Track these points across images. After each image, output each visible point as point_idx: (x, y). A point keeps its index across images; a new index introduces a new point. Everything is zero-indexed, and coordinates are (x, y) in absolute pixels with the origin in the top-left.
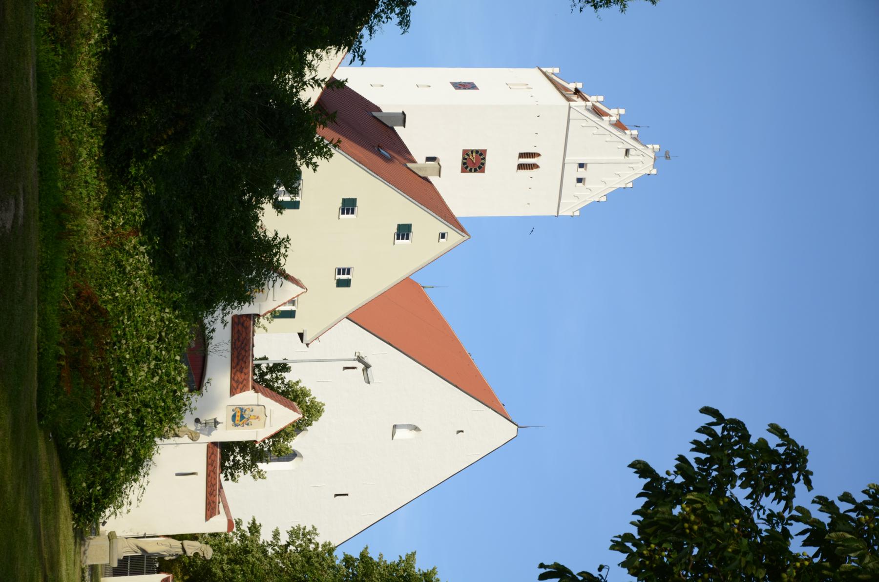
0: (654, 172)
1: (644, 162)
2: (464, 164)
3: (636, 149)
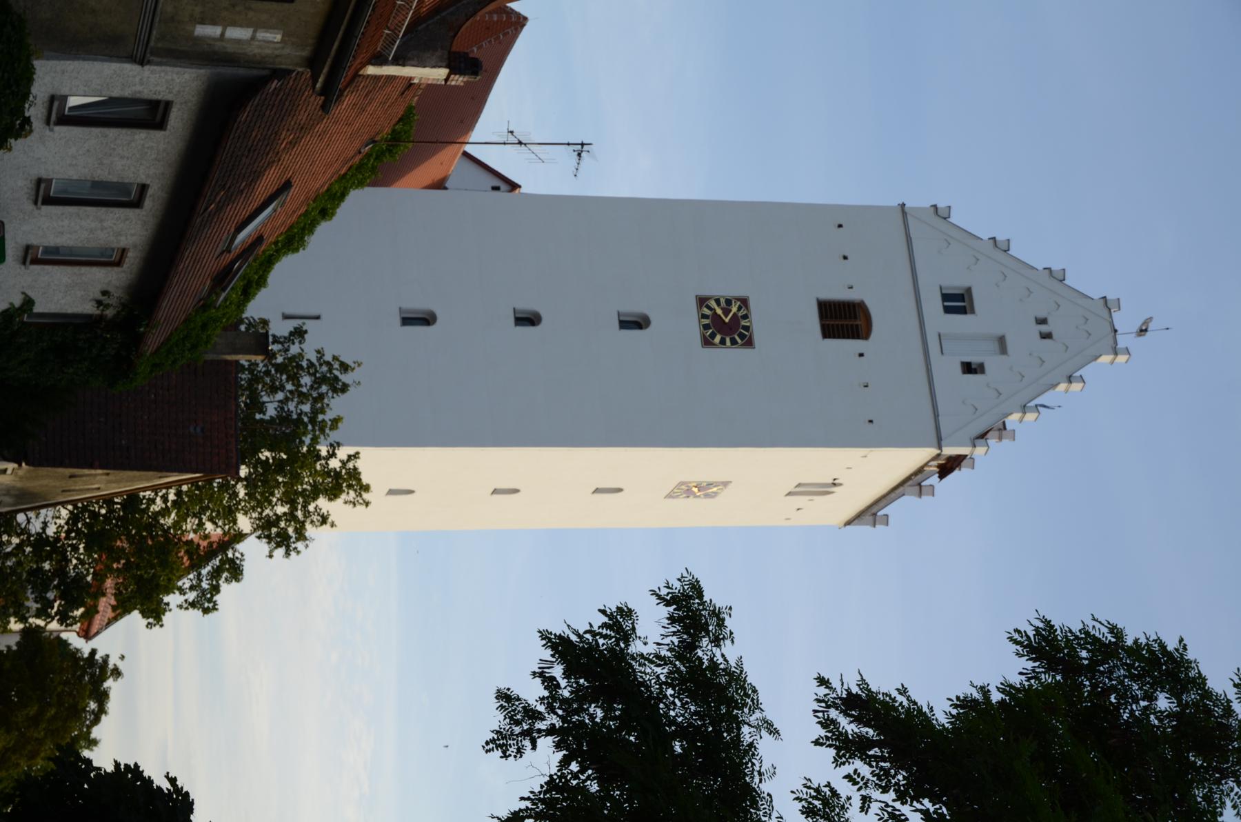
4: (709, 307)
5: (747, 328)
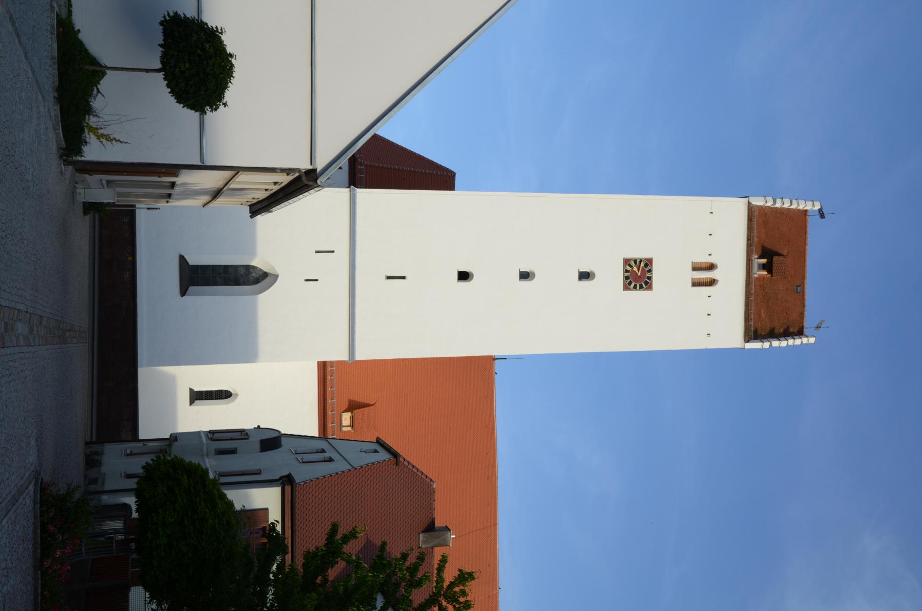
2: (627, 278)
4: (631, 266)
5: (650, 278)
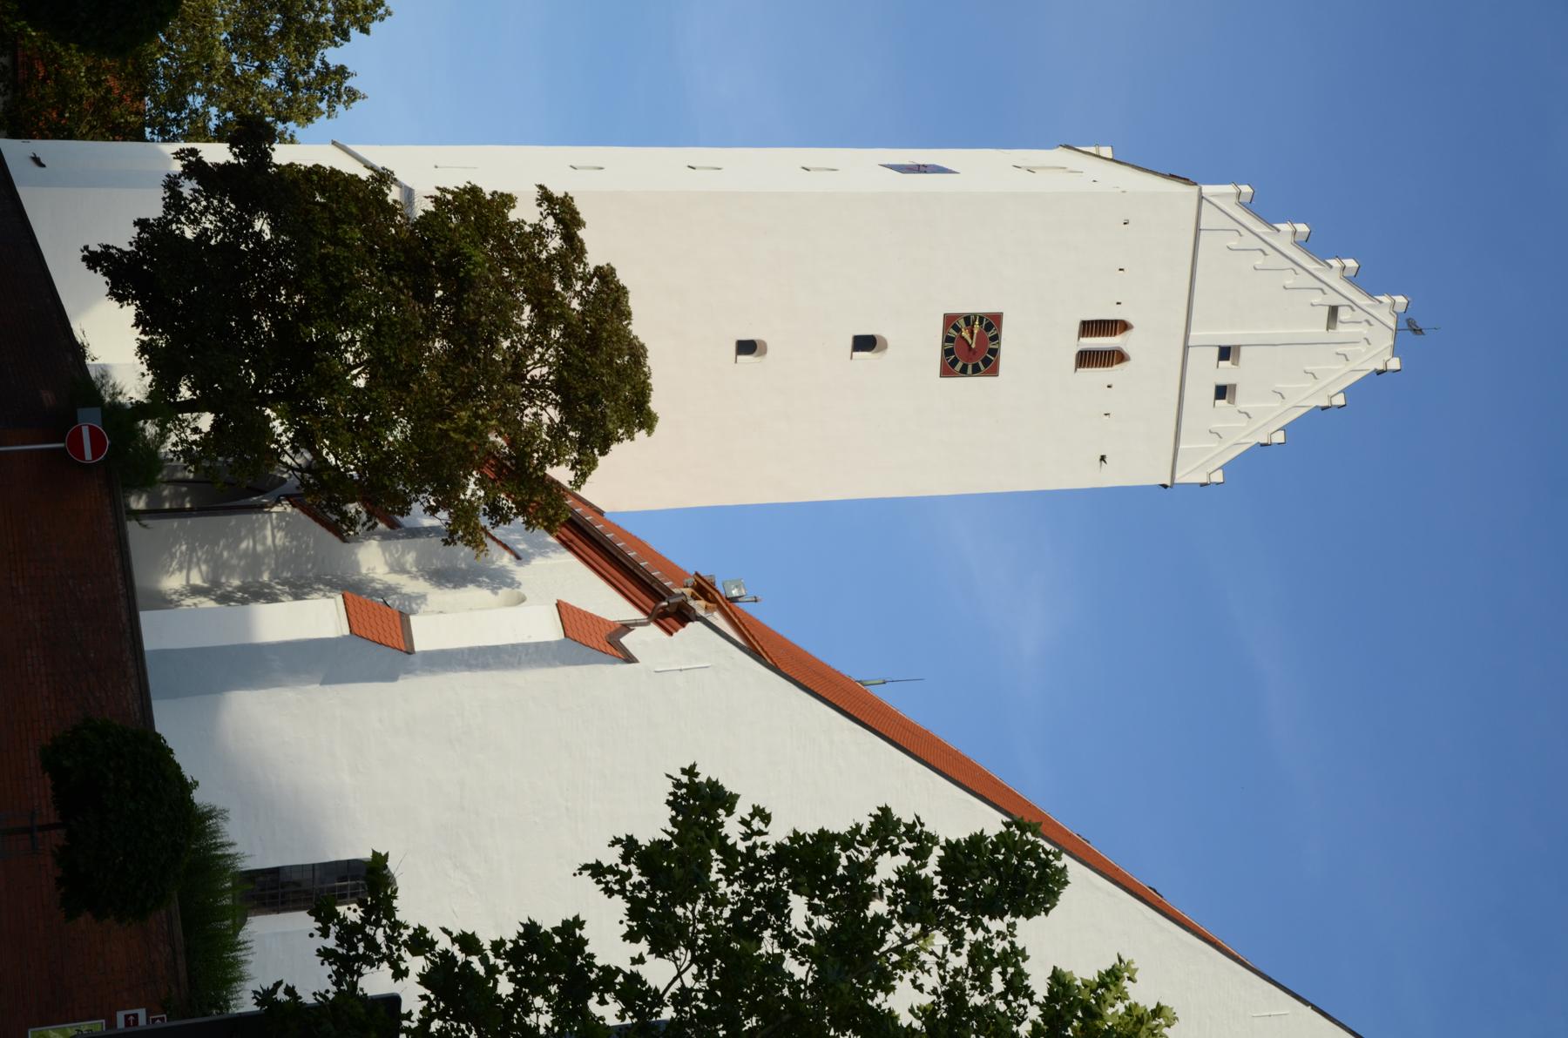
0: (1395, 364)
1: (1369, 341)
2: (947, 353)
3: (1353, 306)
